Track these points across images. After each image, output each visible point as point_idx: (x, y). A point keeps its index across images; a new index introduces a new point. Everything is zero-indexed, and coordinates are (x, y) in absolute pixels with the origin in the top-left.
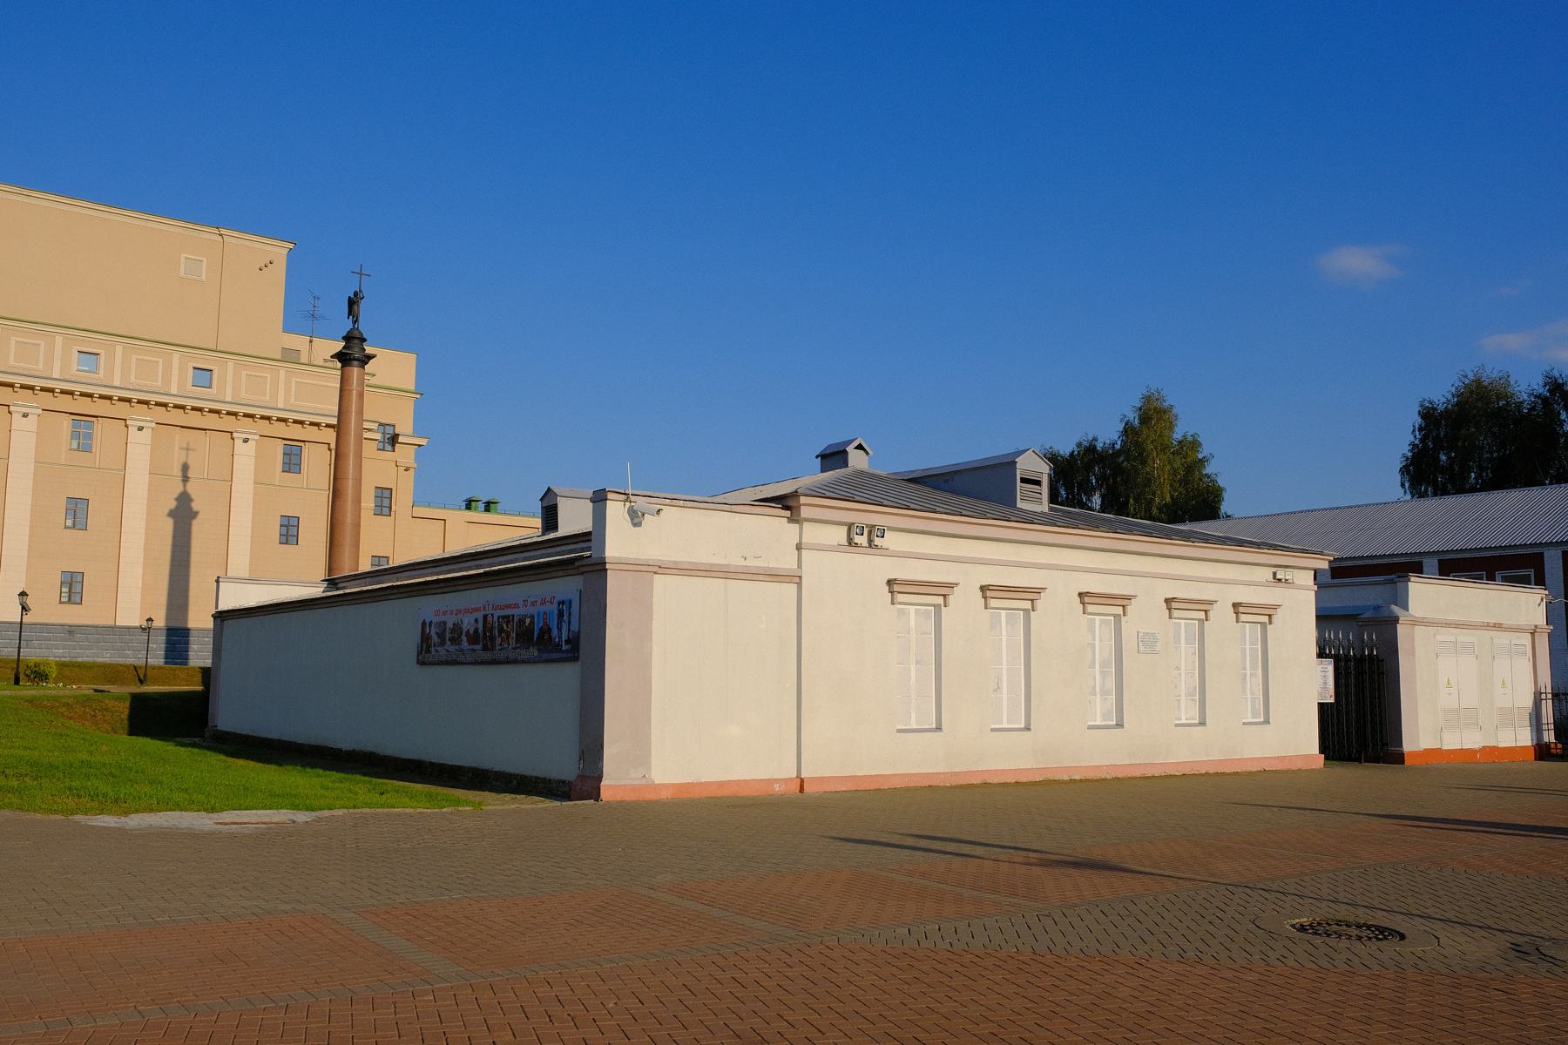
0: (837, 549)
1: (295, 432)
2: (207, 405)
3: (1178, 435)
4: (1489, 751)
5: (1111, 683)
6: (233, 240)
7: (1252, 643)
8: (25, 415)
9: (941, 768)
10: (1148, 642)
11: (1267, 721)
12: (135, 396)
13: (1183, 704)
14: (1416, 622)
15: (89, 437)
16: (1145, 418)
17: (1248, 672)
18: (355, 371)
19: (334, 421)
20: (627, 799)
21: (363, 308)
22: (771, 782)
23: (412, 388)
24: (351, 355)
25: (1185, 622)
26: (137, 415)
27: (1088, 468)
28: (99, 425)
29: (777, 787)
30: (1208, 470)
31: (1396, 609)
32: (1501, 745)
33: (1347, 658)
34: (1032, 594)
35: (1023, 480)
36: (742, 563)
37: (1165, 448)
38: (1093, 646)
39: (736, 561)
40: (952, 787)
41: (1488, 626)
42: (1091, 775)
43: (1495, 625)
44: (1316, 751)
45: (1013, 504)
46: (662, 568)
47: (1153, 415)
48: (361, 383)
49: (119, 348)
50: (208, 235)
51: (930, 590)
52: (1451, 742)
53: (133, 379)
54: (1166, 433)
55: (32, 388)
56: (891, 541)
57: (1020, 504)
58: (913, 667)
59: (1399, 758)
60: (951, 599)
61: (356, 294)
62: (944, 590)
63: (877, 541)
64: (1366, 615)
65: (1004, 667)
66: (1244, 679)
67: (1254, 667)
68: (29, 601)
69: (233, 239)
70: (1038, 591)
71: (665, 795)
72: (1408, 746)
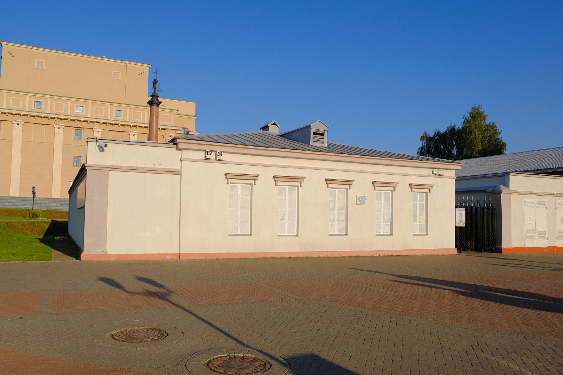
0: (200, 160)
1: (78, 124)
2: (120, 123)
3: (487, 122)
4: (551, 249)
5: (343, 217)
6: (130, 65)
7: (421, 201)
8: (59, 128)
9: (297, 250)
10: (362, 200)
11: (427, 234)
12: (95, 120)
13: (382, 226)
14: (512, 193)
15: (81, 135)
16: (473, 117)
17: (418, 213)
18: (155, 108)
19: (148, 126)
20: (93, 260)
21: (157, 85)
22: (166, 255)
23: (194, 115)
24: (154, 102)
25: (383, 192)
26: (16, 119)
27: (451, 138)
28: (84, 131)
29: (168, 257)
30: (499, 137)
31: (502, 187)
32: (559, 246)
33: (471, 208)
34: (254, 177)
35: (314, 133)
36: (154, 166)
37: (479, 128)
38: (334, 202)
39: (150, 166)
40: (256, 259)
41: (553, 195)
42: (329, 255)
43: (557, 194)
44: (454, 247)
45: (308, 143)
46: (112, 169)
47: (476, 115)
48: (157, 112)
49: (90, 104)
50: (121, 63)
51: (389, 185)
52: (530, 244)
53: (11, 106)
54: (482, 122)
55: (136, 126)
56: (225, 157)
57: (312, 143)
58: (239, 210)
59: (500, 251)
60: (431, 190)
61: (155, 80)
62: (394, 185)
63: (218, 157)
64: (490, 190)
65: (287, 210)
66: (415, 216)
67: (421, 211)
68: (36, 191)
69: (130, 64)
70: (303, 178)
71: (113, 259)
72: (505, 245)
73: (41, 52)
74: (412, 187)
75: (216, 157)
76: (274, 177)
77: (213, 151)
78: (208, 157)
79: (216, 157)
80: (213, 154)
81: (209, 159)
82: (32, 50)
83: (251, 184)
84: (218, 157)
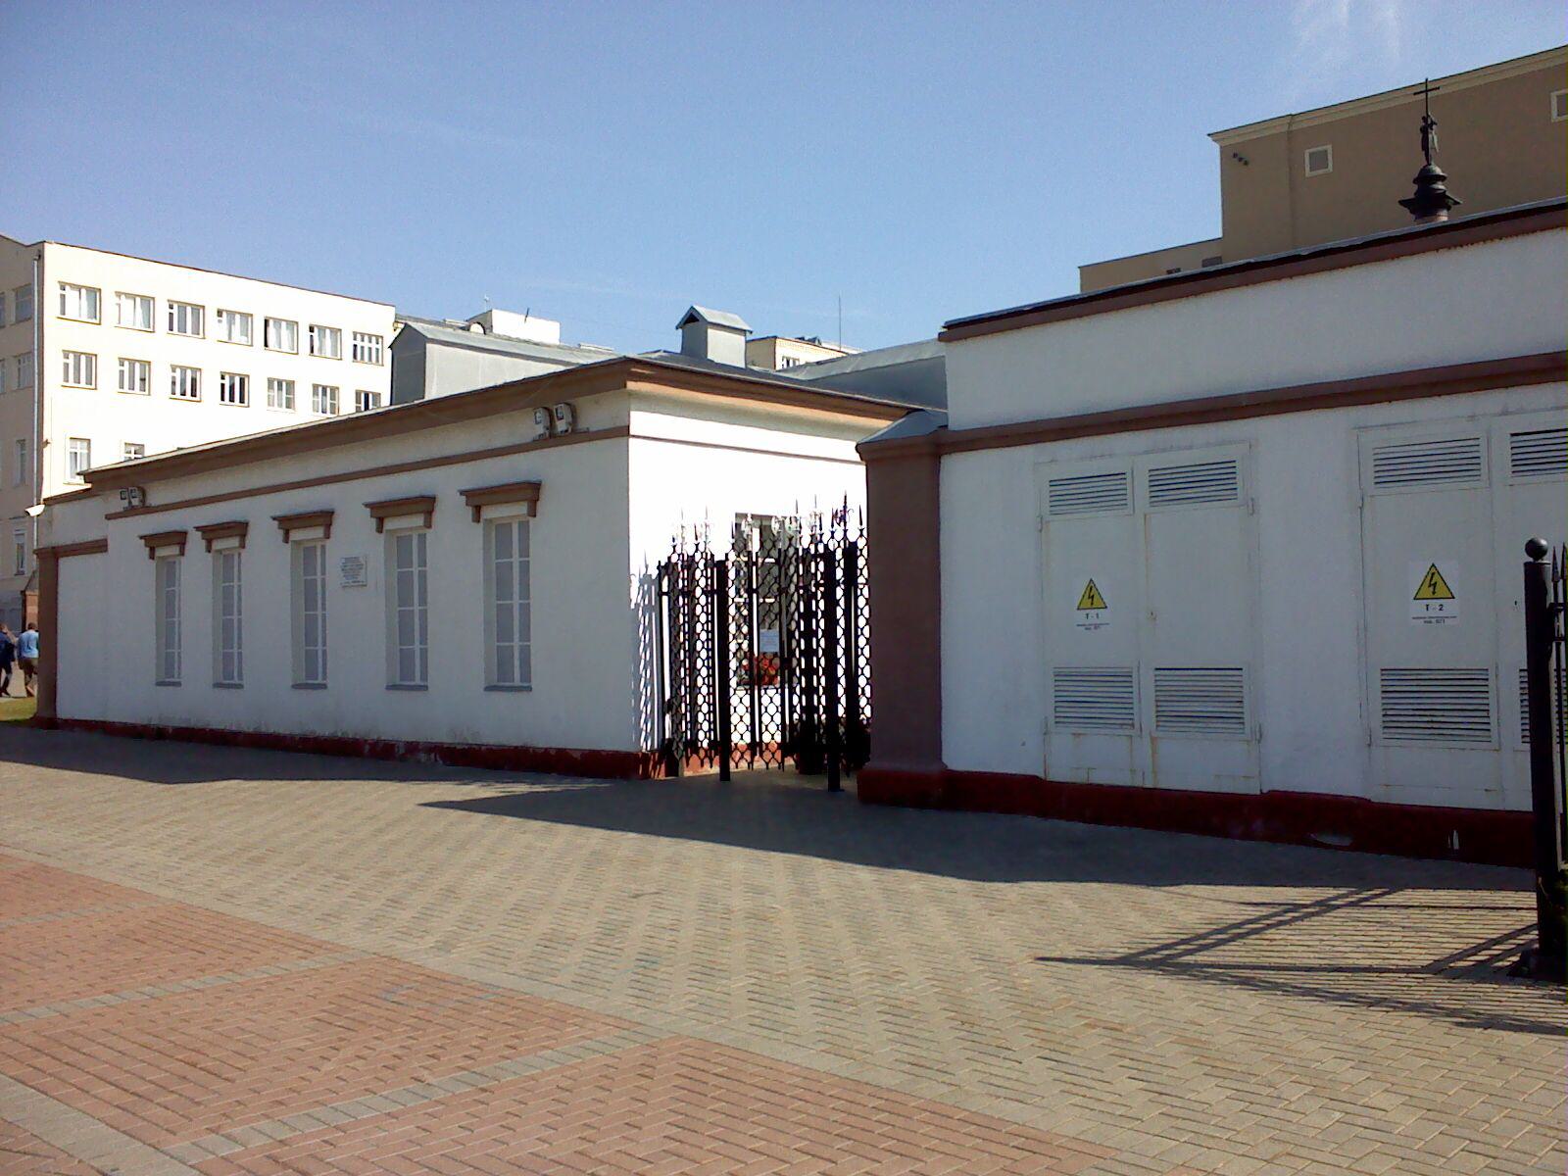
10: (353, 568)
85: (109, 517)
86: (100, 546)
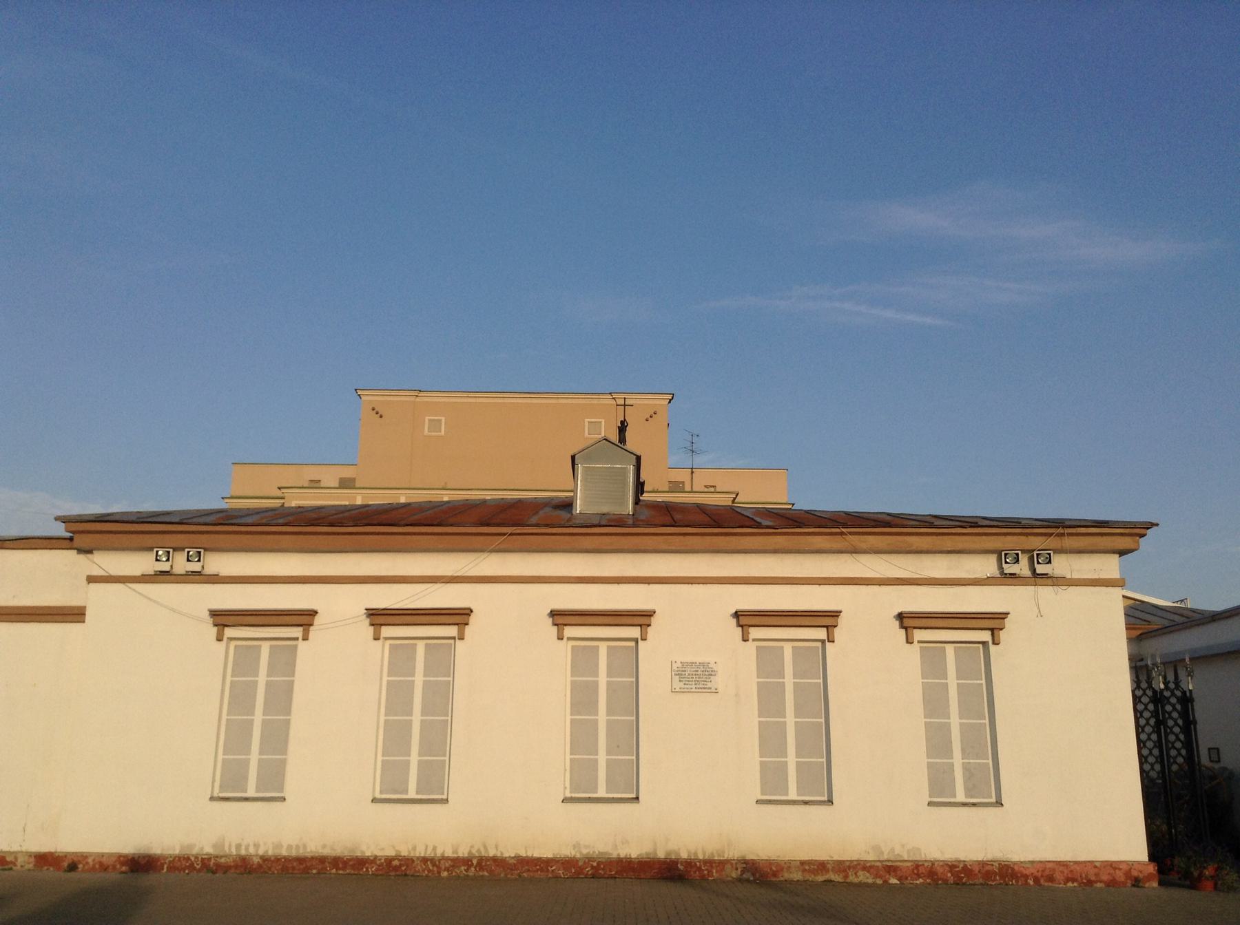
10: (696, 677)
29: (223, 860)
73: (391, 398)
74: (907, 622)
75: (1034, 570)
76: (737, 615)
77: (1023, 551)
78: (1008, 569)
79: (1034, 570)
80: (1024, 560)
81: (1013, 575)
82: (418, 399)
83: (984, 643)
84: (1040, 569)
85: (91, 579)
86: (75, 615)
